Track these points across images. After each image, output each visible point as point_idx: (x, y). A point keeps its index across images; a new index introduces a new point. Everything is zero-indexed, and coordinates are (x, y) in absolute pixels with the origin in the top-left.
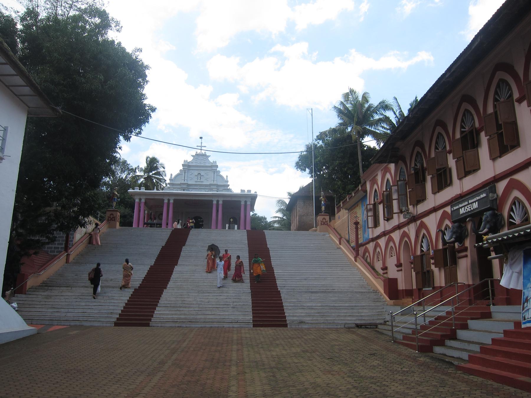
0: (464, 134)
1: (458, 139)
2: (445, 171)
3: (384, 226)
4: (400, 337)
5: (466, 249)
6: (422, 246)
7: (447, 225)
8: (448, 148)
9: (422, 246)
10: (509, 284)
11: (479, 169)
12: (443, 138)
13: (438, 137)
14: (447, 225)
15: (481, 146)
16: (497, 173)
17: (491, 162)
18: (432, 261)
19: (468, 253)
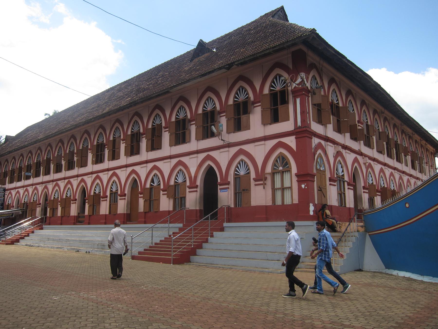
0: (133, 133)
1: (129, 135)
2: (72, 162)
3: (90, 167)
4: (136, 254)
5: (197, 187)
6: (34, 198)
7: (98, 183)
8: (122, 137)
9: (34, 198)
10: (196, 207)
11: (87, 166)
12: (103, 136)
13: (71, 144)
14: (98, 183)
15: (142, 142)
16: (148, 159)
17: (262, 126)
18: (59, 203)
19: (198, 189)
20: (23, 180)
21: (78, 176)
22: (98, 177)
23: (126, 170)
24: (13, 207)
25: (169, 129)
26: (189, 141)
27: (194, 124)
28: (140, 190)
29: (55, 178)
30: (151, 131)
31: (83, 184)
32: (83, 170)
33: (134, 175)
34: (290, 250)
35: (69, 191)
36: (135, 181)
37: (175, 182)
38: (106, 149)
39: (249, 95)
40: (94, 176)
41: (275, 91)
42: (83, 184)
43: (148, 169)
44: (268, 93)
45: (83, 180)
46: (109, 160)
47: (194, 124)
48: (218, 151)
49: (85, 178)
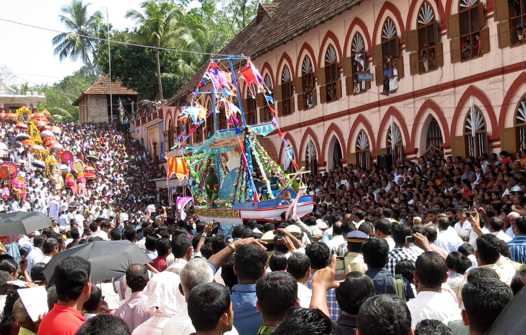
0: (421, 27)
20: (274, 120)
21: (323, 119)
22: (361, 119)
23: (503, 80)
24: (325, 164)
25: (496, 12)
26: (488, 50)
27: (445, 34)
28: (444, 142)
29: (353, 106)
30: (457, 19)
31: (334, 133)
32: (333, 107)
33: (430, 111)
34: (271, 271)
35: (363, 139)
36: (432, 124)
37: (517, 121)
38: (445, 37)
39: (396, 32)
40: (354, 117)
41: (466, 10)
42: (334, 133)
43: (459, 97)
44: (457, 13)
45: (333, 127)
46: (300, 109)
47: (445, 34)
48: (485, 81)
49: (337, 121)
